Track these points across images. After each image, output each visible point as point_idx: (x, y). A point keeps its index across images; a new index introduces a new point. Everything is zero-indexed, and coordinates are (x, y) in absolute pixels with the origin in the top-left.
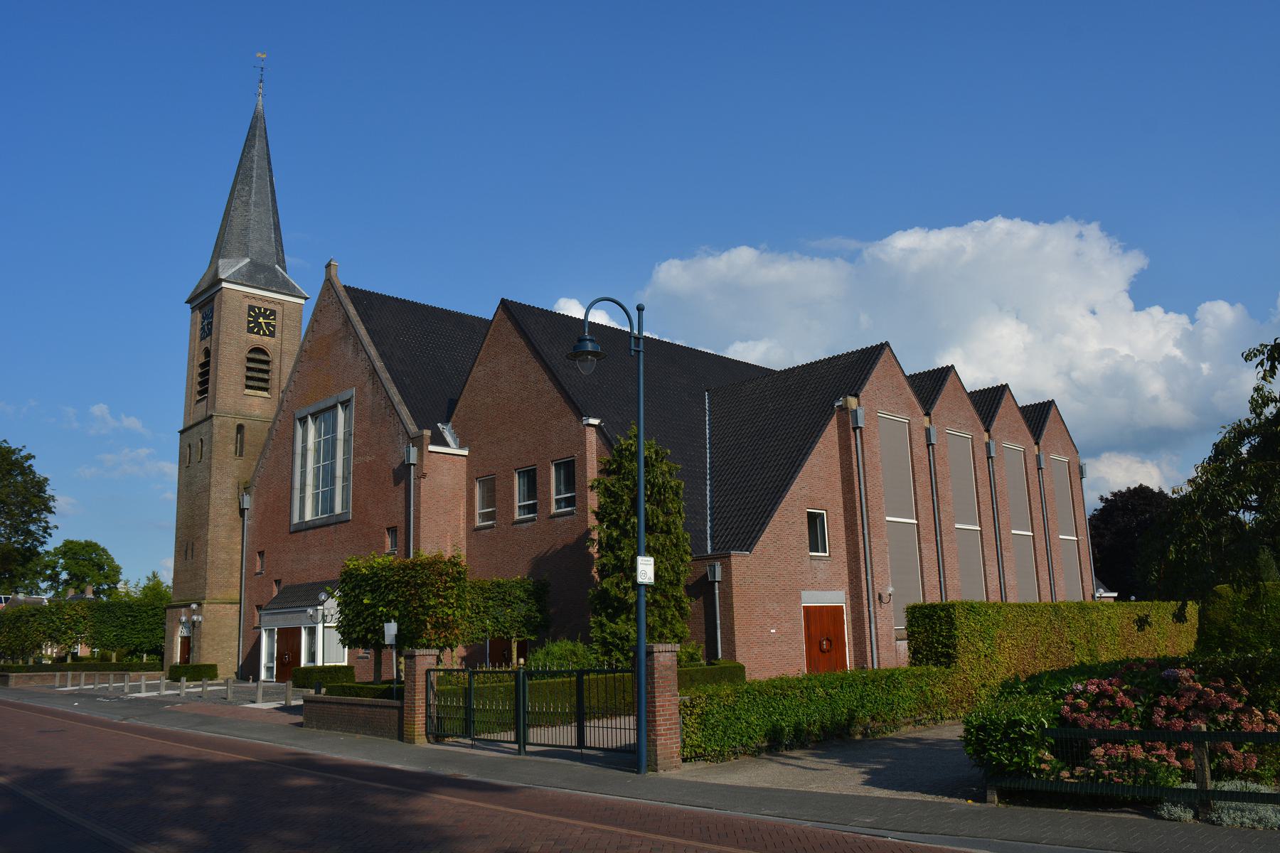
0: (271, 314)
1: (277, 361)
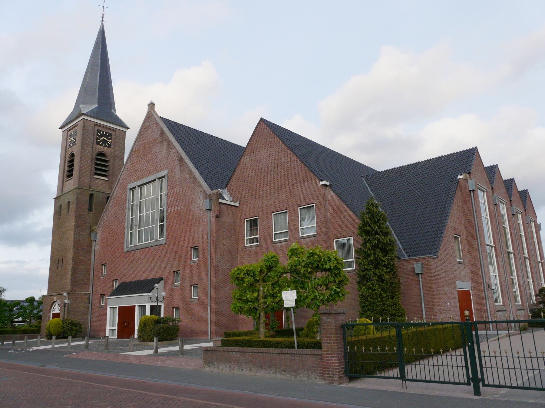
0: (109, 136)
1: (112, 161)
